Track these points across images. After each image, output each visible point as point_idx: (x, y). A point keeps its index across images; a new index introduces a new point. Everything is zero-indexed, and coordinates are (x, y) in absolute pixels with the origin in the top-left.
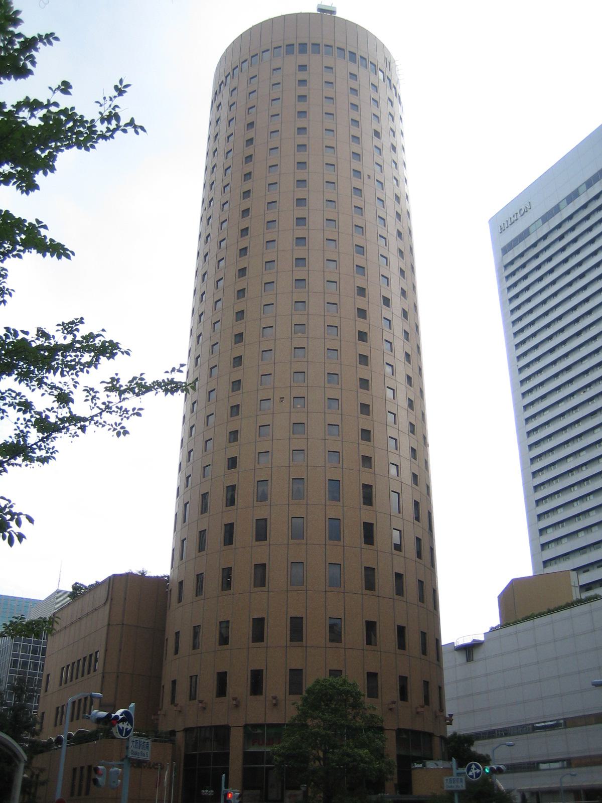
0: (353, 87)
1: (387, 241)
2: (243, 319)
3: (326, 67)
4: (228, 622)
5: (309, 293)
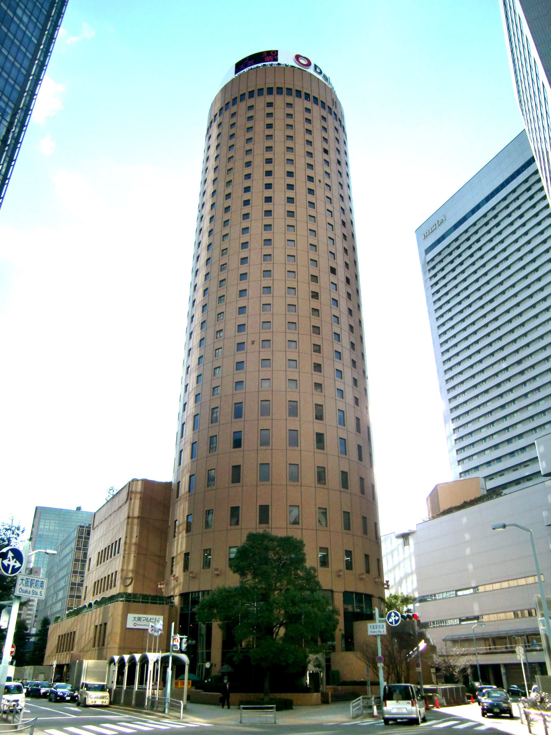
0: (307, 117)
3: (288, 255)
4: (210, 549)
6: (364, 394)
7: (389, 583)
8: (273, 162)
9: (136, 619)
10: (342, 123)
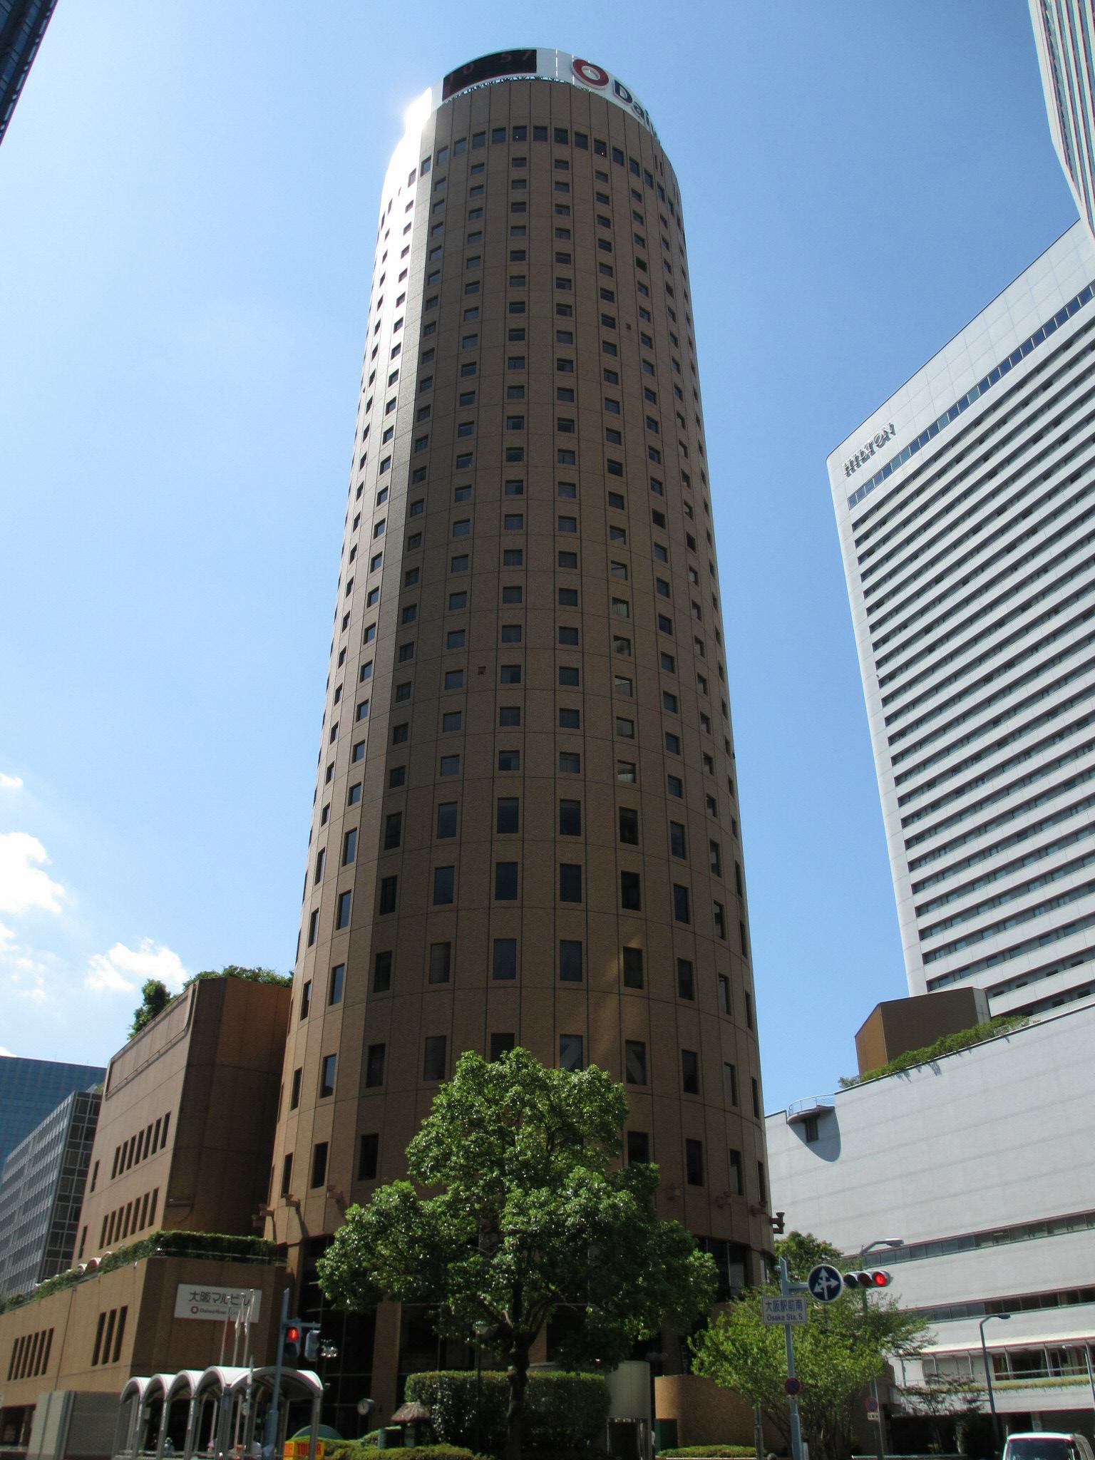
1: (668, 554)
2: (406, 740)
5: (529, 501)
7: (785, 1219)
8: (526, 310)
9: (198, 1297)
10: (676, 207)
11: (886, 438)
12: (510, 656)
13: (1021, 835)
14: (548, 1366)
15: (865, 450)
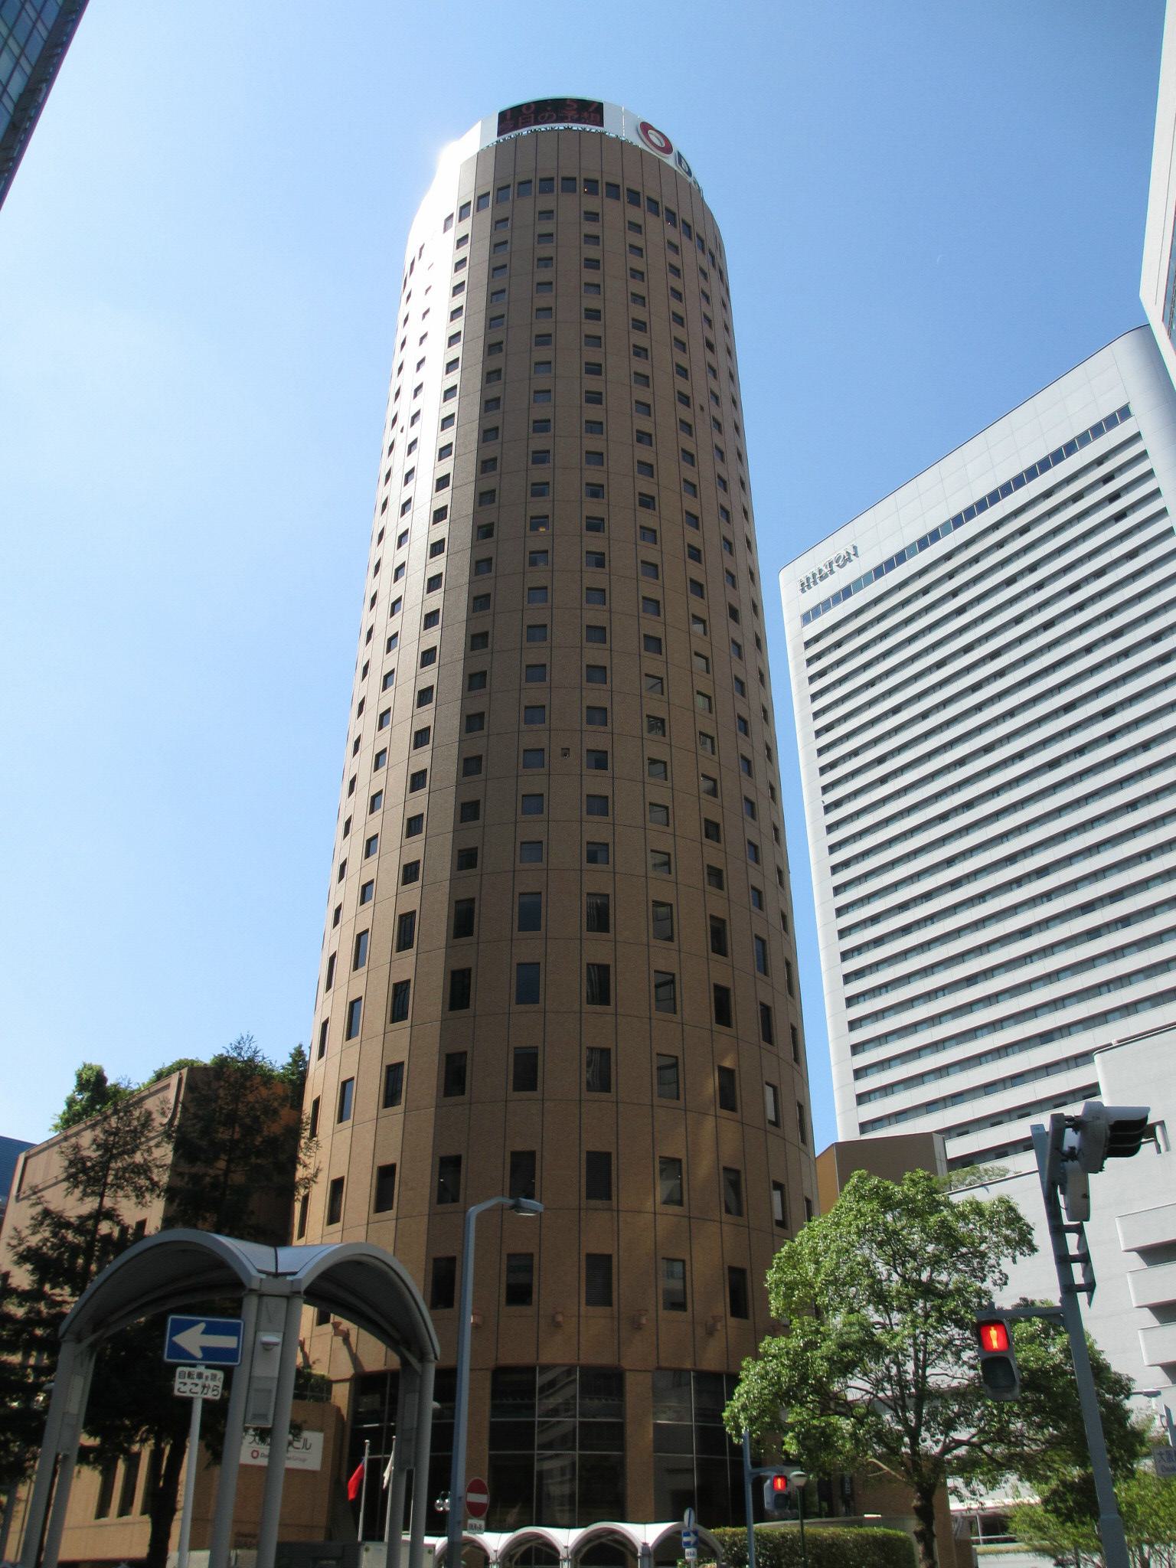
6: (785, 990)
11: (848, 559)
12: (596, 740)
13: (971, 980)
14: (827, 1522)
15: (824, 568)
